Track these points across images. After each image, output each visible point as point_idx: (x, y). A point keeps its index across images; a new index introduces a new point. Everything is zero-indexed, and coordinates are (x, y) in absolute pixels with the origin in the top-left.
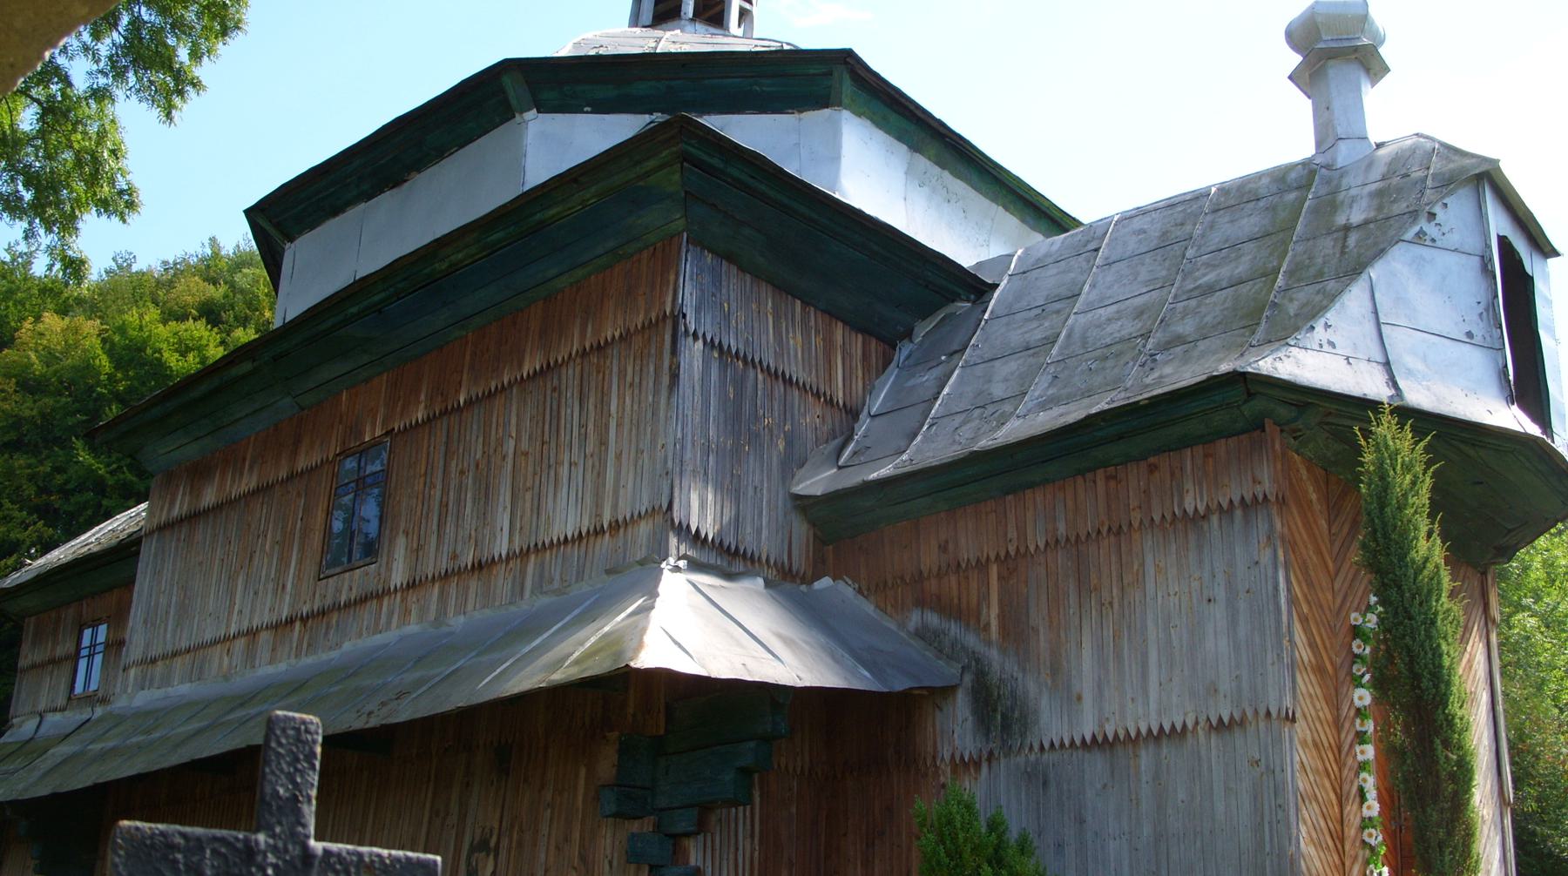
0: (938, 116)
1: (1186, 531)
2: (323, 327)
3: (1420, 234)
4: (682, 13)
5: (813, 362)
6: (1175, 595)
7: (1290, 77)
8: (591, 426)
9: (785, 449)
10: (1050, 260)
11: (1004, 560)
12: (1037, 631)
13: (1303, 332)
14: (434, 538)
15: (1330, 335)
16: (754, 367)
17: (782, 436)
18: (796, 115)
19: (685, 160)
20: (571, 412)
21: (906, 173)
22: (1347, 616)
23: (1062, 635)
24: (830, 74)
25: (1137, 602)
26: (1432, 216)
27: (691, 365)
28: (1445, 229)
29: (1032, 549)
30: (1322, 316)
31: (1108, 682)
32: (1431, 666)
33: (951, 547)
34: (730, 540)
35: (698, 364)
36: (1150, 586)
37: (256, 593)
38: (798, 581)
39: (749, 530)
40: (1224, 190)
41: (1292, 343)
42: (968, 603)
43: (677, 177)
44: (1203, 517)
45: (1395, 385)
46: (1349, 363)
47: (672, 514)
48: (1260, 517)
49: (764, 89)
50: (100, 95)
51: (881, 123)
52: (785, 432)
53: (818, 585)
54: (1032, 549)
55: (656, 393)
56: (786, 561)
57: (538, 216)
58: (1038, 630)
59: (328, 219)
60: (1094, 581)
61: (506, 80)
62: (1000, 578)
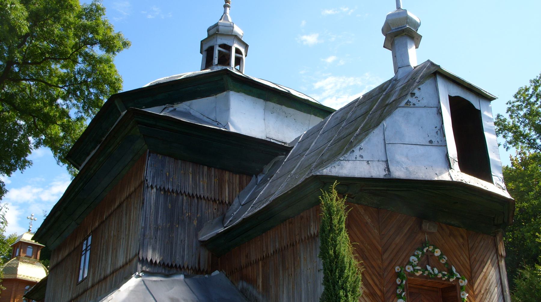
1: (312, 242)
3: (408, 102)
4: (213, 63)
5: (213, 189)
6: (309, 269)
7: (384, 47)
8: (127, 225)
9: (197, 224)
11: (263, 259)
13: (348, 154)
15: (362, 153)
16: (182, 195)
17: (196, 219)
18: (215, 96)
22: (393, 268)
25: (299, 273)
26: (413, 94)
27: (150, 198)
28: (419, 99)
30: (359, 145)
34: (168, 261)
35: (153, 197)
36: (302, 268)
37: (66, 291)
43: (138, 130)
44: (317, 236)
45: (389, 170)
46: (368, 164)
51: (249, 93)
52: (197, 218)
53: (213, 274)
55: (139, 211)
56: (197, 267)
61: (116, 102)
62: (262, 266)
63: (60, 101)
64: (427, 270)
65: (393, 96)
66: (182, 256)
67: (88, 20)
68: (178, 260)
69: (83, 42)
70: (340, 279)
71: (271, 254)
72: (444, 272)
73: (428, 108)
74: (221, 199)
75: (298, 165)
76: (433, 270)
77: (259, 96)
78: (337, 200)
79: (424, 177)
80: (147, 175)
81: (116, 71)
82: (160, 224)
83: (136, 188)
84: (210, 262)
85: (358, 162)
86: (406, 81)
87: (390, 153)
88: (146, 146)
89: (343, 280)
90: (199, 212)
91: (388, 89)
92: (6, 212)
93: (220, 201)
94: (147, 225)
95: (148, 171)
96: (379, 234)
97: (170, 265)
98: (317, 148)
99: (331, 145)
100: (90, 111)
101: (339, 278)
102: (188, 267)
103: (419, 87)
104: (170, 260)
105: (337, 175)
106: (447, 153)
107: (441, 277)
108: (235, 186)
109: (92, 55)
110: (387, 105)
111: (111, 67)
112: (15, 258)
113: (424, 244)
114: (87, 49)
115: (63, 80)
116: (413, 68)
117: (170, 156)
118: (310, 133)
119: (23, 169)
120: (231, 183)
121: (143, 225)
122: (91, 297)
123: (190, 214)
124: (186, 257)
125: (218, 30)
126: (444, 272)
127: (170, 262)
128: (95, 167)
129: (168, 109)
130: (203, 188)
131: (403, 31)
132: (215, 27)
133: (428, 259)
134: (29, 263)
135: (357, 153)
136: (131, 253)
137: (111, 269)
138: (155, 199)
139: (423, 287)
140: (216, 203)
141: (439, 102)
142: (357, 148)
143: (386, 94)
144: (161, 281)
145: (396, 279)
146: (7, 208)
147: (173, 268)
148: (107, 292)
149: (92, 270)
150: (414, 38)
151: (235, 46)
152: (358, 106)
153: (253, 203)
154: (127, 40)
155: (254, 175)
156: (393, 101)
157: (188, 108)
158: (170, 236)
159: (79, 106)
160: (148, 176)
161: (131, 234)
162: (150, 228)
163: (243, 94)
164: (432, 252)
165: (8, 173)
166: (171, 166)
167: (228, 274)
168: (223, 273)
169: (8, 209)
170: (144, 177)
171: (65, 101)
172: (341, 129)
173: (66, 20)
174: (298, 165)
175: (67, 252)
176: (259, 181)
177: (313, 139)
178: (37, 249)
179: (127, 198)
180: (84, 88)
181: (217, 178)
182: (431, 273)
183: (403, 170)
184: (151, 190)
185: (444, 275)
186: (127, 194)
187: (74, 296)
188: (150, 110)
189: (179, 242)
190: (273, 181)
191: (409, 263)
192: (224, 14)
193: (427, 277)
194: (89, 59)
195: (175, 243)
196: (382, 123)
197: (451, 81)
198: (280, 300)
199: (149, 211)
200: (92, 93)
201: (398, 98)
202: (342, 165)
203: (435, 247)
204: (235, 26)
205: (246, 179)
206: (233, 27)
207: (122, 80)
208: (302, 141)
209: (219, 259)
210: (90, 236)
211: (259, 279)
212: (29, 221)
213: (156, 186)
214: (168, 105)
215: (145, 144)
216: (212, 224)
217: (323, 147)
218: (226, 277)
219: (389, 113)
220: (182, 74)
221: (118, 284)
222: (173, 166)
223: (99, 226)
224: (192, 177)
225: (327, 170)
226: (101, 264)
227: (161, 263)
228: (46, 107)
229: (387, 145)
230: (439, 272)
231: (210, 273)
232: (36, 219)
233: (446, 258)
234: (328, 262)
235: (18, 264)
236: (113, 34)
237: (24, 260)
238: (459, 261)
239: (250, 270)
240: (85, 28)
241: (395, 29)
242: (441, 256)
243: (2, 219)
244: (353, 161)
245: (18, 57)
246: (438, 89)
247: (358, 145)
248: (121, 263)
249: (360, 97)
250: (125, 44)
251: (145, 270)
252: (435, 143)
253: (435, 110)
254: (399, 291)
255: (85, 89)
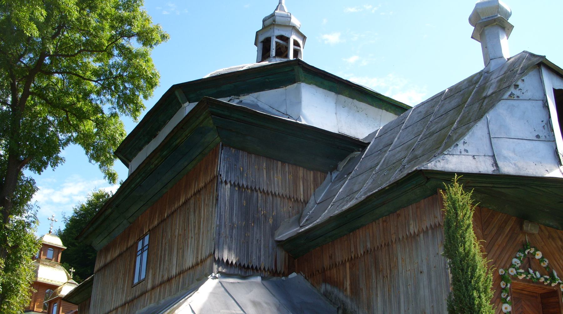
0: (345, 79)
1: (412, 241)
2: (126, 193)
3: (511, 95)
5: (287, 185)
6: (409, 271)
7: (472, 37)
8: (196, 222)
9: (273, 223)
10: (389, 129)
12: (362, 290)
13: (452, 148)
14: (158, 269)
15: (466, 147)
16: (256, 191)
17: (271, 217)
18: (284, 88)
19: (213, 114)
20: (192, 217)
21: (335, 103)
23: (371, 292)
24: (293, 70)
26: (516, 86)
28: (523, 91)
29: (359, 255)
31: (387, 311)
32: (468, 304)
33: (333, 257)
34: (244, 262)
36: (400, 268)
37: (118, 294)
38: (281, 275)
39: (254, 257)
40: (451, 89)
41: (446, 153)
42: (340, 280)
43: (211, 121)
44: (418, 235)
45: (497, 165)
46: (474, 158)
47: (215, 255)
48: (438, 233)
49: (270, 80)
50: (114, 115)
51: (320, 85)
52: (273, 216)
53: (290, 276)
54: (359, 255)
55: (212, 208)
56: (274, 268)
57: (174, 144)
58: (362, 290)
59: (139, 152)
60: (381, 267)
61: (177, 93)
62: (350, 268)
63: (93, 96)
64: (529, 273)
65: (490, 89)
66: (258, 256)
67: (125, 11)
68: (254, 260)
69: (120, 33)
70: (472, 278)
71: (361, 254)
72: (546, 277)
73: (533, 101)
74: (296, 197)
75: (382, 161)
76: (535, 274)
77: (331, 89)
78: (462, 194)
79: (534, 173)
80: (221, 170)
81: (153, 65)
82: (235, 222)
83: (207, 183)
84: (287, 264)
85: (464, 156)
86: (502, 72)
87: (496, 147)
88: (219, 138)
89: (475, 279)
90: (274, 209)
91: (480, 81)
92: (37, 211)
93: (295, 199)
94: (222, 222)
95: (221, 165)
96: (482, 234)
97: (246, 266)
98: (402, 143)
99: (421, 139)
100: (125, 107)
101: (472, 278)
102: (264, 269)
103: (523, 79)
104: (246, 261)
105: (443, 170)
106: (557, 148)
107: (543, 281)
108: (309, 183)
109: (128, 48)
110: (485, 98)
111: (148, 61)
112: (36, 260)
113: (524, 247)
114: (123, 41)
115: (96, 73)
116: (507, 60)
117: (243, 149)
118: (388, 128)
119: (54, 166)
120: (305, 180)
121: (218, 223)
122: (151, 300)
123: (265, 212)
124: (262, 258)
125: (274, 21)
126: (546, 277)
127: (246, 262)
128: (157, 162)
129: (233, 101)
130: (278, 185)
131: (495, 20)
132: (271, 17)
133: (529, 262)
134: (49, 266)
135: (461, 147)
136: (203, 252)
137: (177, 270)
138: (229, 195)
139: (524, 292)
140: (291, 200)
141: (545, 95)
142: (460, 142)
143: (479, 86)
144: (238, 282)
145: (500, 282)
146: (38, 207)
147: (249, 270)
148: (172, 294)
149: (151, 271)
150: (506, 28)
151: (293, 37)
152: (445, 99)
153: (333, 201)
154: (166, 33)
155: (329, 172)
156: (492, 94)
157: (256, 100)
158: (246, 235)
159: (114, 101)
160: (221, 171)
161: (201, 233)
162: (225, 226)
163: (314, 86)
164: (534, 255)
165: (39, 170)
166: (244, 161)
167: (308, 277)
168: (302, 275)
169: (40, 208)
170: (218, 173)
171: (99, 95)
172: (429, 123)
173: (102, 9)
174: (382, 161)
175: (117, 252)
176: (333, 178)
177: (394, 135)
178: (58, 252)
179: (195, 194)
180: (119, 82)
181: (292, 174)
182: (533, 277)
183: (512, 166)
184: (225, 186)
185: (546, 279)
186: (194, 190)
187: (128, 299)
188: (224, 100)
189: (255, 242)
190: (352, 178)
191: (512, 266)
192: (279, 4)
193: (530, 281)
194: (125, 52)
195: (251, 243)
196: (485, 115)
197: (554, 73)
198: (373, 303)
199: (224, 208)
200: (127, 88)
201: (498, 90)
202: (447, 160)
203: (537, 250)
204: (292, 16)
205: (321, 176)
206: (290, 18)
207: (160, 76)
208: (380, 136)
209: (296, 260)
210: (146, 236)
211: (346, 281)
212: (50, 222)
213: (230, 182)
214: (233, 96)
215: (218, 137)
216: (289, 222)
217: (412, 141)
218: (305, 279)
219: (492, 105)
220: (244, 65)
221: (187, 285)
222: (246, 161)
223: (158, 224)
224: (266, 172)
225: (431, 164)
226: (164, 265)
227: (237, 264)
228: (80, 102)
229: (492, 139)
230: (541, 276)
231: (287, 276)
232: (57, 220)
233: (547, 261)
234: (459, 261)
235: (38, 267)
236: (151, 26)
237: (45, 263)
238: (559, 265)
239: (335, 271)
240: (121, 20)
241: (485, 18)
242: (542, 260)
243: (34, 218)
244: (457, 156)
245: (51, 49)
246: (543, 81)
247: (461, 138)
248: (190, 263)
249: (445, 90)
250: (164, 37)
251: (221, 271)
252: (543, 138)
253: (540, 103)
254: (504, 295)
255: (120, 84)
